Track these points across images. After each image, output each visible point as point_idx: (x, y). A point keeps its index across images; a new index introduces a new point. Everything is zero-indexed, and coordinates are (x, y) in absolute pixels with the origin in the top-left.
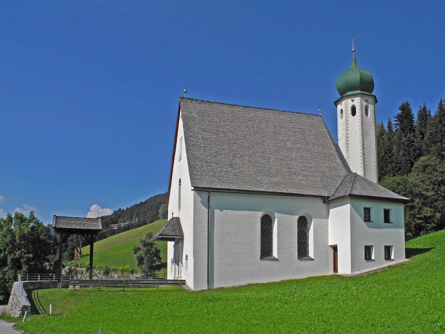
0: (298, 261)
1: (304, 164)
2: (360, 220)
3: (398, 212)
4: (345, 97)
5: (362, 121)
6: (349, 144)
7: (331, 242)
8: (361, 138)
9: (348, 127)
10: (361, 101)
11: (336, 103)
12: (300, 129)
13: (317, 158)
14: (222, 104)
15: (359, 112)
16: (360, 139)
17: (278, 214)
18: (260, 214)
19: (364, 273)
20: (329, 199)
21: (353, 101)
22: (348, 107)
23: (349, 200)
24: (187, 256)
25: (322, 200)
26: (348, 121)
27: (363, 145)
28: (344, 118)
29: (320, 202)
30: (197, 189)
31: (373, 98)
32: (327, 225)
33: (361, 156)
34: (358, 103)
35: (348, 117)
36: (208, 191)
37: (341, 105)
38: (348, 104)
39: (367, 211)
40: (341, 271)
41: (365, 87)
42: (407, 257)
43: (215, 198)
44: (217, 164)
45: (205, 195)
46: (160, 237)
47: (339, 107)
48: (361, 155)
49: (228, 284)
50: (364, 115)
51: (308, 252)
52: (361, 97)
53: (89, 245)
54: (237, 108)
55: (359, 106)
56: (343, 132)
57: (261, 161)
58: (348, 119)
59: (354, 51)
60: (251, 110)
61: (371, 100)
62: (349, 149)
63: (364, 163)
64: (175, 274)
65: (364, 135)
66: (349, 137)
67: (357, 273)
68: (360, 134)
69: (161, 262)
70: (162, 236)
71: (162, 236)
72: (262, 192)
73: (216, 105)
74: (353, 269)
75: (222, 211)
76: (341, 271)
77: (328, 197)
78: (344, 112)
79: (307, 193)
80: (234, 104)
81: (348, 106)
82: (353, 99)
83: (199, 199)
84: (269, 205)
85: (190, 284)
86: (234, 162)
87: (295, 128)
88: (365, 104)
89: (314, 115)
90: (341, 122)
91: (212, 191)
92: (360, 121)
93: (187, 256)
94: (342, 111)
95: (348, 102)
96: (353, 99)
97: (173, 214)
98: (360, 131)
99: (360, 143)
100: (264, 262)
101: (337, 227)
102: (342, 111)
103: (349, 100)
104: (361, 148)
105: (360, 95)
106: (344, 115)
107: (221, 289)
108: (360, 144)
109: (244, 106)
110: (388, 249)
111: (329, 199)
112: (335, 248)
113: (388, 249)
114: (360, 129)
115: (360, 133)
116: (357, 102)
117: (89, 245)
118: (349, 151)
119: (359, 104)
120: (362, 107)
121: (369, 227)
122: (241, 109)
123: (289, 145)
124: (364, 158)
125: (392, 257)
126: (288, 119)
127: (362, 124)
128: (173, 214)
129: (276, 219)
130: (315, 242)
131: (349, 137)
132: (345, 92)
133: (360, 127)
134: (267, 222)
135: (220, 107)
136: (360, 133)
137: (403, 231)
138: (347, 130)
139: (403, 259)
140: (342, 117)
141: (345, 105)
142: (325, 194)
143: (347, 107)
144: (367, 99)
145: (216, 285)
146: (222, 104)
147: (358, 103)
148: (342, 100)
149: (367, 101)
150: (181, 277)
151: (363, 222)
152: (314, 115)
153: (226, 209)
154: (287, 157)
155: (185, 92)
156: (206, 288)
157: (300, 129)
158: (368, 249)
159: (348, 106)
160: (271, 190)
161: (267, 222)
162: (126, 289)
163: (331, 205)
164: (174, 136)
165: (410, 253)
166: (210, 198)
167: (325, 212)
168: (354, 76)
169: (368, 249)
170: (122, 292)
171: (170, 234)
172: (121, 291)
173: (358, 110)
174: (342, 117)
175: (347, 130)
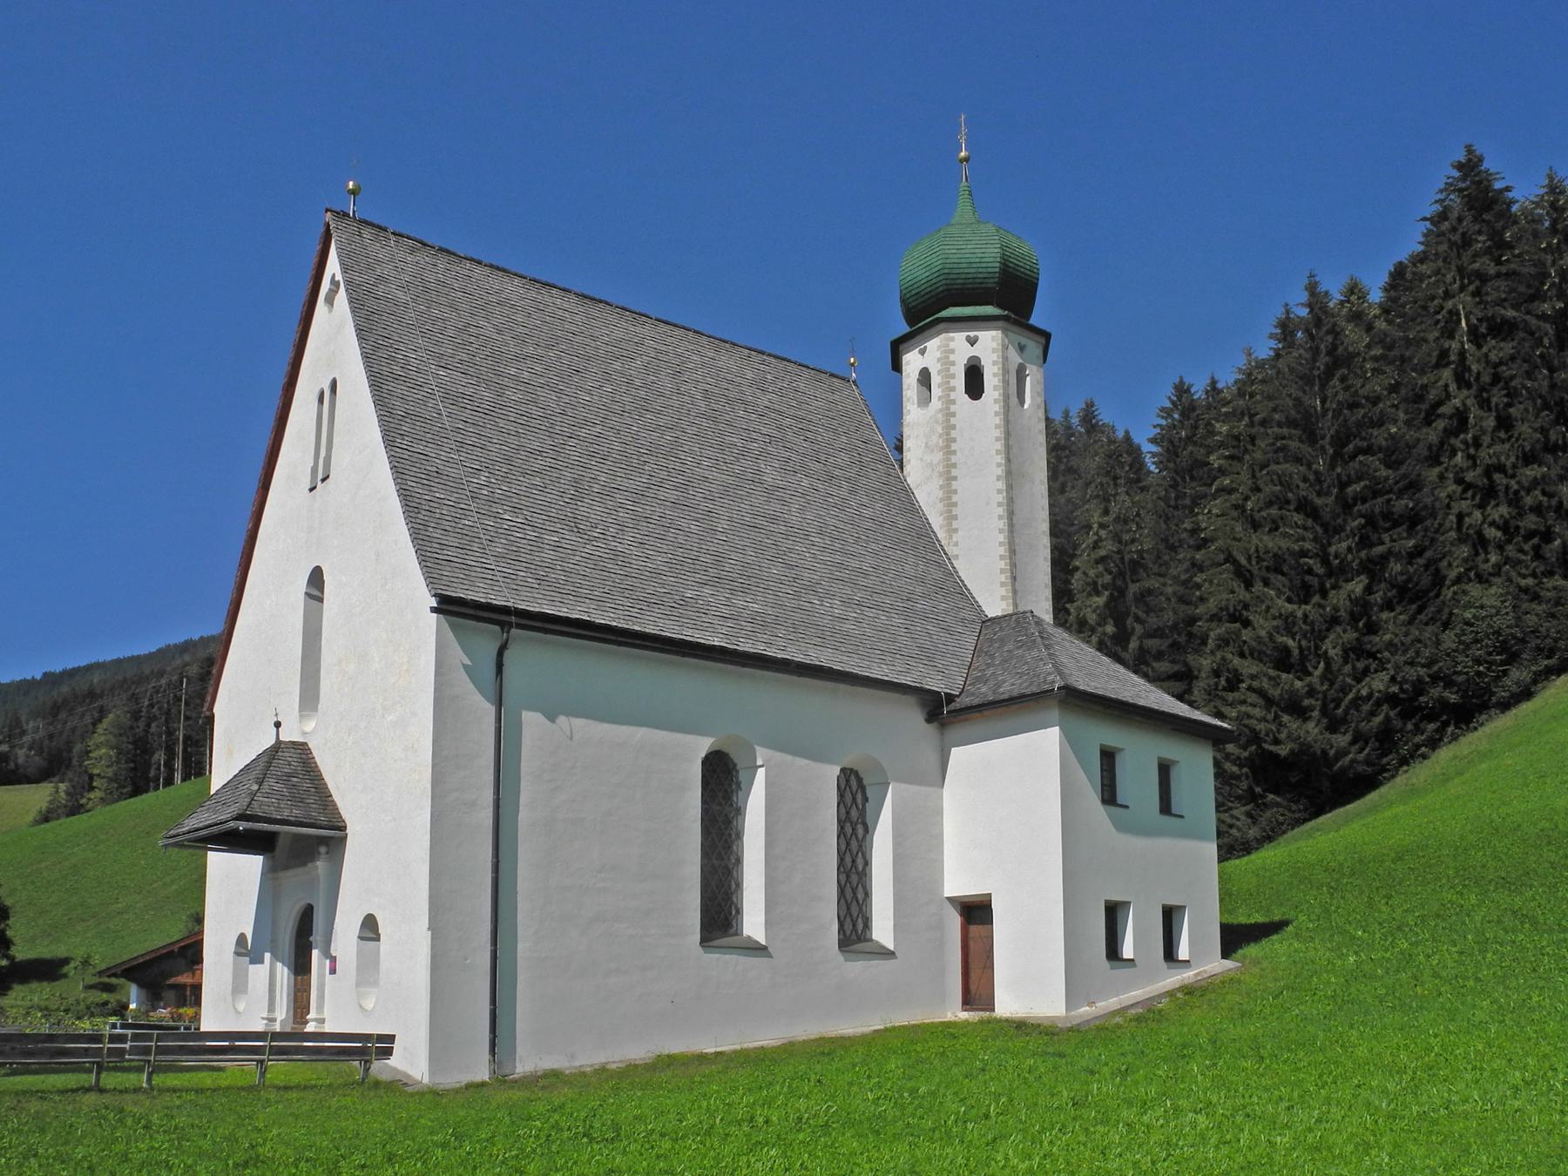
0: (841, 958)
1: (838, 558)
2: (1091, 796)
3: (1197, 770)
4: (942, 326)
5: (1007, 422)
6: (955, 504)
7: (957, 884)
8: (1001, 485)
9: (954, 440)
10: (1005, 348)
11: (897, 350)
12: (794, 417)
13: (876, 541)
14: (498, 269)
15: (995, 388)
16: (999, 491)
17: (769, 752)
18: (704, 745)
19: (1114, 1013)
20: (952, 706)
21: (972, 342)
22: (953, 363)
23: (1055, 713)
24: (370, 928)
25: (923, 704)
26: (954, 415)
27: (1011, 514)
28: (936, 403)
29: (912, 717)
30: (448, 606)
31: (1043, 340)
32: (939, 812)
33: (1002, 558)
34: (994, 351)
35: (953, 402)
36: (502, 624)
37: (923, 352)
38: (952, 351)
39: (1108, 757)
40: (1007, 1004)
41: (1009, 296)
42: (1226, 954)
43: (532, 659)
44: (515, 509)
45: (486, 639)
46: (242, 826)
47: (913, 362)
48: (1002, 551)
49: (573, 1057)
50: (1014, 400)
51: (867, 925)
52: (1005, 331)
53: (524, 713)
54: (553, 299)
55: (995, 363)
56: (928, 458)
57: (683, 524)
58: (953, 408)
59: (967, 159)
60: (612, 317)
61: (1034, 348)
62: (955, 525)
63: (1013, 585)
64: (271, 1009)
65: (1012, 477)
66: (955, 478)
67: (1085, 1011)
68: (1000, 471)
69: (11, 959)
70: (249, 825)
71: (249, 825)
72: (712, 649)
73: (478, 271)
74: (1072, 998)
75: (553, 721)
76: (1007, 1004)
77: (950, 698)
78: (936, 380)
79: (876, 673)
80: (544, 279)
81: (952, 357)
82: (972, 334)
83: (458, 656)
84: (738, 702)
85: (411, 1060)
86: (583, 510)
87: (780, 413)
88: (1015, 359)
89: (833, 375)
90: (917, 419)
91: (519, 626)
92: (998, 420)
93: (370, 928)
94: (925, 377)
95: (952, 345)
96: (972, 334)
97: (278, 725)
98: (1000, 459)
99: (999, 504)
100: (714, 956)
101: (1000, 819)
102: (925, 377)
103: (958, 339)
104: (1002, 524)
105: (1000, 323)
106: (936, 391)
107: (554, 1078)
108: (1000, 511)
109: (585, 297)
110: (1170, 916)
111: (952, 706)
112: (976, 912)
113: (1170, 916)
114: (998, 452)
115: (999, 465)
116: (990, 345)
117: (524, 713)
118: (956, 530)
119: (995, 357)
120: (1005, 371)
121: (1121, 827)
122: (571, 303)
123: (770, 476)
124: (1013, 565)
125: (1183, 952)
126: (749, 375)
127: (1008, 435)
128: (278, 725)
129: (761, 773)
130: (898, 880)
131: (955, 478)
132: (926, 311)
133: (999, 445)
134: (722, 779)
135: (496, 282)
136: (999, 465)
137: (1211, 849)
138: (948, 451)
139: (1216, 965)
140: (925, 401)
141: (941, 353)
142: (936, 684)
143: (946, 362)
144: (1024, 341)
145: (527, 1062)
146: (498, 269)
147: (994, 351)
148: (926, 333)
149: (1021, 348)
150: (322, 1021)
151: (1099, 802)
152: (833, 375)
153: (567, 715)
154: (774, 519)
155: (353, 192)
156: (483, 1075)
157: (794, 417)
158: (1114, 913)
159: (952, 357)
160: (746, 646)
161: (722, 779)
162: (110, 1080)
163: (954, 732)
164: (283, 380)
165: (1234, 938)
166: (507, 654)
167: (932, 758)
168: (974, 244)
169: (1114, 913)
170: (91, 1098)
171: (286, 814)
172: (87, 1090)
173: (991, 380)
174: (925, 401)
175: (948, 451)
